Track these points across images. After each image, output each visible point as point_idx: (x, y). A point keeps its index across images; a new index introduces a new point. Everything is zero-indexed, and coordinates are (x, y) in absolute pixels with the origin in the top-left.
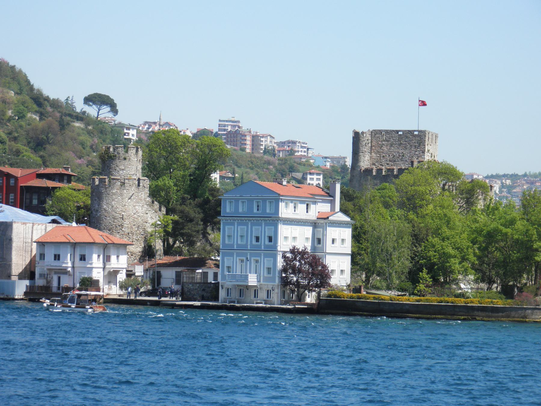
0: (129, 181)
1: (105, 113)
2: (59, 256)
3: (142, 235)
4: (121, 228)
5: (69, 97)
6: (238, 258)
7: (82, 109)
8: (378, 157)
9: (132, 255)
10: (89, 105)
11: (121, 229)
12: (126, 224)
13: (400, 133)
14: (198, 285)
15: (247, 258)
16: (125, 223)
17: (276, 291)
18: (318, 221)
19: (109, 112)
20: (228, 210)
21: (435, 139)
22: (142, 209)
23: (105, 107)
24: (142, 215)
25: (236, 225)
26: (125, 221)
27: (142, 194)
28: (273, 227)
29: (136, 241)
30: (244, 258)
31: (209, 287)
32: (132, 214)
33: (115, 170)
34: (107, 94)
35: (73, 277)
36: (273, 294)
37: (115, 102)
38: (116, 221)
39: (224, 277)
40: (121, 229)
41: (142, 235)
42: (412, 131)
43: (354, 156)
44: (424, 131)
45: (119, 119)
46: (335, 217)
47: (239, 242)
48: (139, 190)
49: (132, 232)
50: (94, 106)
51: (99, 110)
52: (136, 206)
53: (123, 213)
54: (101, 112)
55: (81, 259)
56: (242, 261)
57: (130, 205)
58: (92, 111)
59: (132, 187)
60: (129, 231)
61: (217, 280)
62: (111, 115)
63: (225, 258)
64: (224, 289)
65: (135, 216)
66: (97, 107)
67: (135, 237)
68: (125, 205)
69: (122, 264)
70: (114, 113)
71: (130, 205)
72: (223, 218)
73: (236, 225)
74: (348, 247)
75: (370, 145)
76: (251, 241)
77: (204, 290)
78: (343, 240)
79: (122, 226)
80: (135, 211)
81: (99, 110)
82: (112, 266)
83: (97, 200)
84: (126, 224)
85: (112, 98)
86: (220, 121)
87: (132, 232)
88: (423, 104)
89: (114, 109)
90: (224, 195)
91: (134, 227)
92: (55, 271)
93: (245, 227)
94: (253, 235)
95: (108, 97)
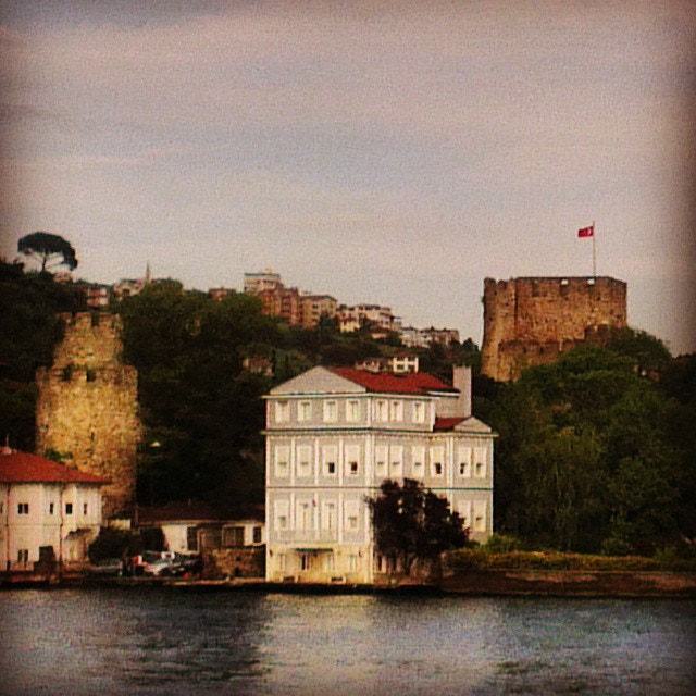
1: (56, 264)
2: (26, 506)
10: (27, 253)
13: (565, 282)
18: (436, 434)
19: (62, 263)
20: (279, 419)
23: (55, 254)
31: (248, 554)
39: (273, 534)
44: (619, 282)
45: (77, 275)
47: (300, 474)
56: (306, 506)
58: (33, 263)
61: (260, 541)
62: (65, 269)
74: (486, 474)
75: (514, 303)
80: (113, 426)
86: (247, 275)
88: (582, 233)
89: (71, 259)
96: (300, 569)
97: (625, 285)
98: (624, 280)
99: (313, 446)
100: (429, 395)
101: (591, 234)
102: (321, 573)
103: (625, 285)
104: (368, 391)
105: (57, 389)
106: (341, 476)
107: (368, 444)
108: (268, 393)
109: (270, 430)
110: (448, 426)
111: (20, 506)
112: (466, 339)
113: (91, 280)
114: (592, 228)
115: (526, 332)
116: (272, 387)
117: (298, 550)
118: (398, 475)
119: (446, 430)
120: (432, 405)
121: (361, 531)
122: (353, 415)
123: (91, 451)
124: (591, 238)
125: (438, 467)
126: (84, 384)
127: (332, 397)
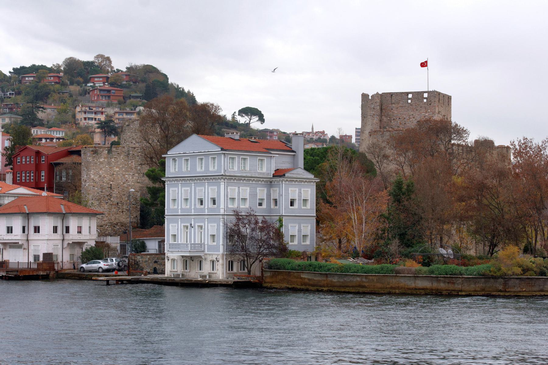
0: (117, 149)
3: (133, 204)
4: (109, 198)
5: (235, 112)
6: (182, 225)
7: (246, 121)
9: (122, 226)
10: (242, 116)
11: (110, 199)
12: (114, 194)
14: (148, 257)
15: (191, 224)
16: (113, 192)
17: (221, 261)
19: (257, 121)
21: (447, 101)
22: (133, 178)
23: (255, 117)
24: (133, 183)
27: (132, 162)
28: (216, 187)
29: (126, 211)
30: (189, 225)
32: (122, 183)
33: (132, 143)
34: (256, 107)
35: (27, 250)
36: (218, 265)
38: (104, 191)
40: (110, 199)
41: (133, 204)
42: (422, 92)
43: (363, 120)
44: (444, 95)
48: (128, 159)
49: (121, 202)
50: (246, 117)
51: (250, 120)
52: (125, 174)
53: (111, 183)
54: (251, 121)
55: (35, 232)
56: (187, 227)
57: (119, 174)
58: (242, 120)
59: (121, 155)
60: (118, 201)
65: (125, 185)
66: (249, 118)
67: (125, 207)
68: (113, 174)
70: (262, 121)
71: (119, 174)
74: (311, 207)
76: (195, 205)
77: (156, 262)
79: (110, 195)
80: (124, 180)
81: (250, 120)
82: (71, 237)
83: (86, 170)
85: (260, 110)
86: (356, 129)
87: (121, 202)
89: (262, 119)
90: (168, 154)
91: (123, 197)
92: (10, 244)
93: (189, 188)
94: (197, 198)
95: (257, 109)
96: (184, 269)
97: (449, 98)
98: (450, 95)
99: (205, 188)
101: (426, 66)
102: (194, 274)
103: (449, 98)
104: (222, 149)
105: (90, 159)
106: (206, 207)
107: (222, 187)
108: (166, 153)
110: (282, 174)
111: (35, 228)
112: (188, 90)
114: (426, 62)
115: (387, 125)
116: (168, 150)
117: (183, 256)
118: (244, 207)
122: (213, 168)
123: (110, 196)
124: (427, 67)
125: (276, 201)
126: (105, 156)
127: (203, 156)
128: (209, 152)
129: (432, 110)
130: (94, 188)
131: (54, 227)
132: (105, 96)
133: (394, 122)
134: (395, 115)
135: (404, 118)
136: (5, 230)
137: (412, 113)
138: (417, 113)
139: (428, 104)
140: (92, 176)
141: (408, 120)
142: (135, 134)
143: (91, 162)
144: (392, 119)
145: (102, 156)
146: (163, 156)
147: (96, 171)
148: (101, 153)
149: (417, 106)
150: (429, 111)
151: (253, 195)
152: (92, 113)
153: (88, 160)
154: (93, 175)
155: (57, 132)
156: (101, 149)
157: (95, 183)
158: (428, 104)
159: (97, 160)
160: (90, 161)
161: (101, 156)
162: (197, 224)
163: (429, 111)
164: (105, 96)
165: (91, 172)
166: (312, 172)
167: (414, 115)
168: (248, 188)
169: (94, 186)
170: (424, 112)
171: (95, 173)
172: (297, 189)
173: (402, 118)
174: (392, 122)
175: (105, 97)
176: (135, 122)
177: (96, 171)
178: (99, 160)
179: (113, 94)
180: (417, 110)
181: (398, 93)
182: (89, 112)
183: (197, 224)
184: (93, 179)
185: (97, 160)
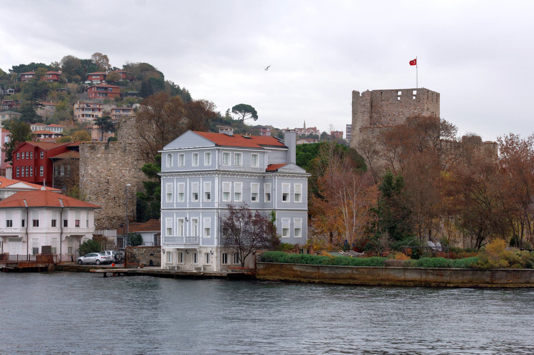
0: (114, 145)
3: (130, 199)
4: (106, 192)
6: (178, 218)
8: (379, 116)
10: (236, 113)
11: (107, 194)
12: (111, 188)
14: (145, 250)
16: (110, 187)
17: (215, 254)
18: (267, 175)
21: (436, 98)
22: (130, 173)
23: (248, 114)
24: (129, 178)
25: (175, 182)
26: (111, 185)
27: (128, 158)
29: (123, 205)
30: (184, 218)
32: (119, 178)
35: (27, 243)
36: (212, 258)
37: (256, 110)
40: (107, 194)
42: (411, 89)
43: (354, 117)
44: (433, 93)
46: (285, 169)
49: (118, 196)
50: (240, 114)
51: (244, 116)
53: (108, 178)
55: (34, 225)
58: (236, 116)
59: (117, 151)
60: (115, 195)
63: (166, 219)
64: (166, 254)
65: (122, 180)
68: (110, 169)
69: (83, 229)
71: (116, 169)
72: (162, 174)
73: (175, 182)
74: (303, 201)
77: (152, 255)
78: (297, 195)
79: (108, 190)
80: (121, 175)
81: (244, 116)
82: (69, 231)
83: (84, 165)
84: (111, 188)
85: (253, 107)
86: (347, 125)
87: (118, 196)
89: (255, 116)
90: (164, 149)
91: (120, 191)
94: (192, 192)
96: (179, 262)
97: (438, 95)
98: (438, 92)
100: (264, 149)
102: (189, 267)
103: (438, 95)
104: (217, 145)
105: (88, 155)
106: (201, 201)
107: (217, 181)
109: (164, 173)
110: (275, 169)
111: (34, 221)
112: (183, 88)
113: (264, 125)
114: (415, 60)
115: (378, 122)
116: (164, 146)
117: (178, 249)
118: (238, 202)
119: (273, 171)
120: (266, 156)
121: (212, 238)
122: (207, 164)
124: (416, 65)
125: (269, 195)
127: (197, 152)
128: (189, 148)
129: (421, 107)
130: (91, 183)
131: (52, 220)
132: (103, 94)
133: (384, 119)
134: (385, 112)
135: (394, 115)
136: (5, 224)
137: (402, 110)
138: (407, 110)
139: (417, 101)
140: (90, 171)
141: (397, 116)
142: (132, 130)
143: (88, 157)
144: (382, 115)
145: (99, 152)
146: (159, 152)
147: (93, 166)
148: (98, 148)
149: (407, 103)
150: (418, 108)
151: (247, 189)
152: (89, 109)
153: (86, 156)
154: (90, 170)
155: (55, 128)
156: (99, 145)
157: (93, 177)
158: (417, 101)
159: (95, 156)
160: (88, 156)
161: (98, 151)
162: (192, 218)
163: (418, 108)
164: (103, 94)
165: (89, 168)
166: (304, 167)
167: (404, 111)
168: (242, 183)
169: (91, 181)
170: (413, 109)
171: (92, 168)
172: (290, 184)
173: (392, 115)
174: (382, 118)
175: (103, 95)
176: (132, 118)
177: (93, 166)
178: (96, 156)
179: (110, 92)
180: (406, 107)
181: (388, 90)
182: (86, 109)
183: (192, 218)
184: (90, 174)
185: (95, 156)
